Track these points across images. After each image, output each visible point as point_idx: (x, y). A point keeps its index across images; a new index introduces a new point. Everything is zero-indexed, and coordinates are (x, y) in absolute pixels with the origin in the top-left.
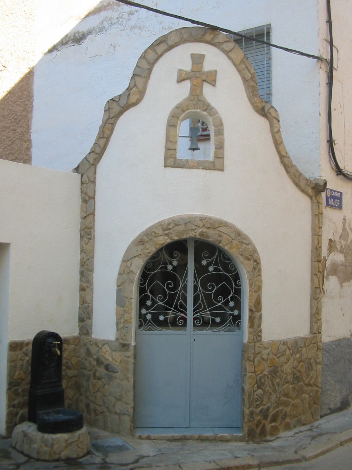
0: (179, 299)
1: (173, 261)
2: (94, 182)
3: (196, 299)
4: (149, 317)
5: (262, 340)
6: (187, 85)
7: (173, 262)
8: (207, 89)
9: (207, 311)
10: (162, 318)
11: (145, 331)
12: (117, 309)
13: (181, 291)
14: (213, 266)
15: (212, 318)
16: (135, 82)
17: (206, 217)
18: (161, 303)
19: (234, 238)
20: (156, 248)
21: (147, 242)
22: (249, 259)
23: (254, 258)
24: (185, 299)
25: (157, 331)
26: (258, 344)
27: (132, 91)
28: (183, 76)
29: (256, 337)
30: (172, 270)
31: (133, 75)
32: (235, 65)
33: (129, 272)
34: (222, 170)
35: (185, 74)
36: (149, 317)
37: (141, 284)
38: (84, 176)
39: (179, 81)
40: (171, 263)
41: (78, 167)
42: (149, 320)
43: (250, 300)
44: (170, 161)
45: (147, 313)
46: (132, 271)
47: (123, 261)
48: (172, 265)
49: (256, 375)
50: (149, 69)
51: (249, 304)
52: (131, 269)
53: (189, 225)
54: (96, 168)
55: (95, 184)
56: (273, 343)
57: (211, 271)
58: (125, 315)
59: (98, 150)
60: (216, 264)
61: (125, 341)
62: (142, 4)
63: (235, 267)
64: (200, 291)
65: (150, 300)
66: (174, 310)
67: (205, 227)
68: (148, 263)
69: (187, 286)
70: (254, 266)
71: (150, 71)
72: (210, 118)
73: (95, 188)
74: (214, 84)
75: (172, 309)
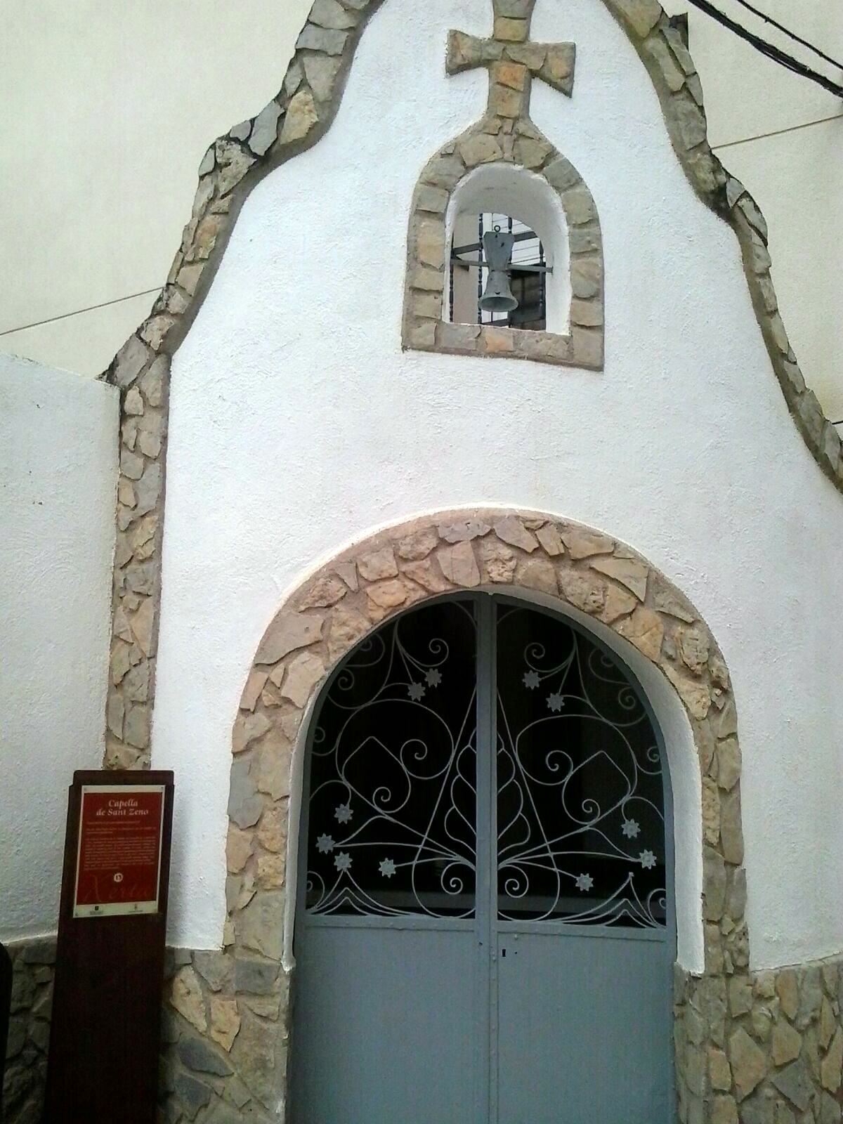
0: (446, 804)
1: (427, 669)
2: (163, 408)
3: (506, 804)
4: (343, 863)
5: (750, 966)
6: (479, 83)
7: (426, 673)
8: (543, 100)
9: (544, 850)
10: (388, 868)
11: (329, 914)
12: (229, 836)
13: (453, 773)
14: (562, 694)
15: (563, 874)
16: (304, 73)
17: (547, 519)
18: (385, 815)
19: (642, 600)
20: (371, 620)
21: (342, 598)
22: (696, 677)
23: (710, 673)
24: (468, 801)
25: (370, 916)
26: (739, 983)
27: (294, 104)
28: (463, 52)
29: (732, 955)
30: (424, 700)
31: (298, 51)
32: (636, 39)
33: (277, 702)
34: (599, 369)
35: (473, 48)
36: (343, 863)
37: (316, 747)
38: (133, 395)
39: (456, 68)
40: (420, 678)
41: (113, 367)
42: (345, 874)
43: (705, 818)
44: (425, 332)
45: (337, 851)
46: (288, 701)
47: (257, 666)
48: (425, 684)
49: (739, 1102)
50: (351, 29)
51: (705, 835)
52: (283, 693)
53: (488, 545)
54: (169, 362)
55: (166, 416)
56: (785, 978)
57: (557, 710)
58: (260, 860)
59: (178, 303)
60: (572, 687)
61: (258, 956)
62: (176, 826)
63: (638, 701)
64: (518, 777)
65: (348, 805)
66: (423, 836)
67: (546, 553)
68: (343, 673)
69: (474, 755)
70: (714, 699)
71: (354, 35)
72: (557, 195)
73: (167, 428)
74: (567, 89)
75: (425, 837)
